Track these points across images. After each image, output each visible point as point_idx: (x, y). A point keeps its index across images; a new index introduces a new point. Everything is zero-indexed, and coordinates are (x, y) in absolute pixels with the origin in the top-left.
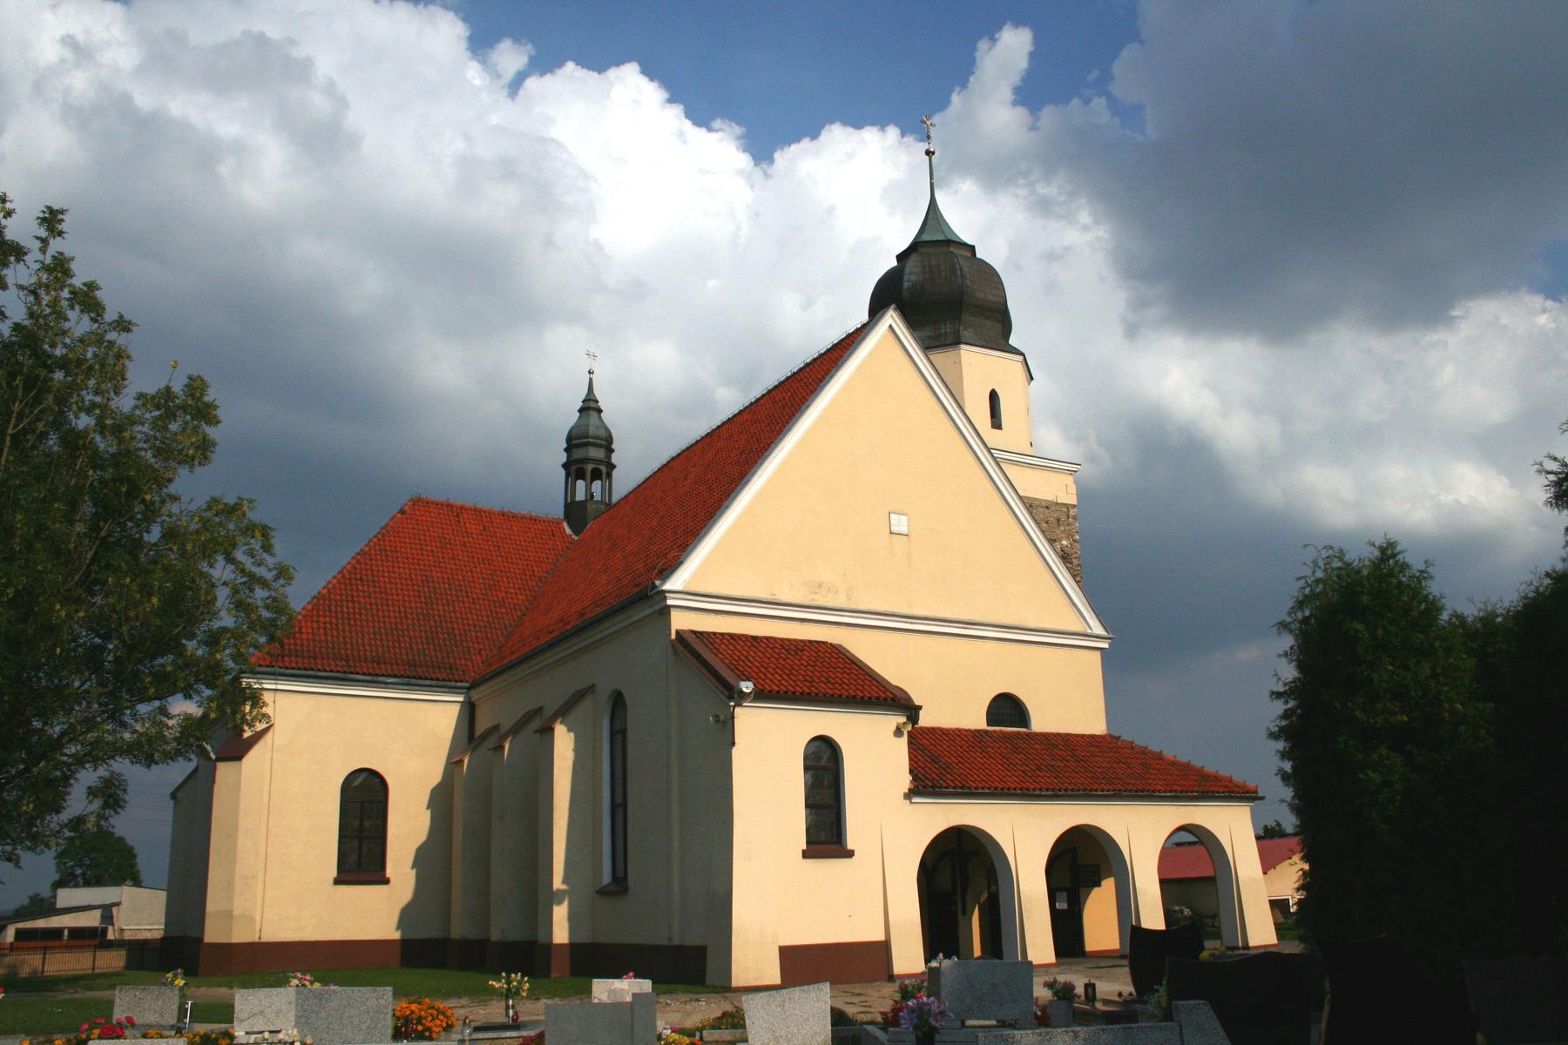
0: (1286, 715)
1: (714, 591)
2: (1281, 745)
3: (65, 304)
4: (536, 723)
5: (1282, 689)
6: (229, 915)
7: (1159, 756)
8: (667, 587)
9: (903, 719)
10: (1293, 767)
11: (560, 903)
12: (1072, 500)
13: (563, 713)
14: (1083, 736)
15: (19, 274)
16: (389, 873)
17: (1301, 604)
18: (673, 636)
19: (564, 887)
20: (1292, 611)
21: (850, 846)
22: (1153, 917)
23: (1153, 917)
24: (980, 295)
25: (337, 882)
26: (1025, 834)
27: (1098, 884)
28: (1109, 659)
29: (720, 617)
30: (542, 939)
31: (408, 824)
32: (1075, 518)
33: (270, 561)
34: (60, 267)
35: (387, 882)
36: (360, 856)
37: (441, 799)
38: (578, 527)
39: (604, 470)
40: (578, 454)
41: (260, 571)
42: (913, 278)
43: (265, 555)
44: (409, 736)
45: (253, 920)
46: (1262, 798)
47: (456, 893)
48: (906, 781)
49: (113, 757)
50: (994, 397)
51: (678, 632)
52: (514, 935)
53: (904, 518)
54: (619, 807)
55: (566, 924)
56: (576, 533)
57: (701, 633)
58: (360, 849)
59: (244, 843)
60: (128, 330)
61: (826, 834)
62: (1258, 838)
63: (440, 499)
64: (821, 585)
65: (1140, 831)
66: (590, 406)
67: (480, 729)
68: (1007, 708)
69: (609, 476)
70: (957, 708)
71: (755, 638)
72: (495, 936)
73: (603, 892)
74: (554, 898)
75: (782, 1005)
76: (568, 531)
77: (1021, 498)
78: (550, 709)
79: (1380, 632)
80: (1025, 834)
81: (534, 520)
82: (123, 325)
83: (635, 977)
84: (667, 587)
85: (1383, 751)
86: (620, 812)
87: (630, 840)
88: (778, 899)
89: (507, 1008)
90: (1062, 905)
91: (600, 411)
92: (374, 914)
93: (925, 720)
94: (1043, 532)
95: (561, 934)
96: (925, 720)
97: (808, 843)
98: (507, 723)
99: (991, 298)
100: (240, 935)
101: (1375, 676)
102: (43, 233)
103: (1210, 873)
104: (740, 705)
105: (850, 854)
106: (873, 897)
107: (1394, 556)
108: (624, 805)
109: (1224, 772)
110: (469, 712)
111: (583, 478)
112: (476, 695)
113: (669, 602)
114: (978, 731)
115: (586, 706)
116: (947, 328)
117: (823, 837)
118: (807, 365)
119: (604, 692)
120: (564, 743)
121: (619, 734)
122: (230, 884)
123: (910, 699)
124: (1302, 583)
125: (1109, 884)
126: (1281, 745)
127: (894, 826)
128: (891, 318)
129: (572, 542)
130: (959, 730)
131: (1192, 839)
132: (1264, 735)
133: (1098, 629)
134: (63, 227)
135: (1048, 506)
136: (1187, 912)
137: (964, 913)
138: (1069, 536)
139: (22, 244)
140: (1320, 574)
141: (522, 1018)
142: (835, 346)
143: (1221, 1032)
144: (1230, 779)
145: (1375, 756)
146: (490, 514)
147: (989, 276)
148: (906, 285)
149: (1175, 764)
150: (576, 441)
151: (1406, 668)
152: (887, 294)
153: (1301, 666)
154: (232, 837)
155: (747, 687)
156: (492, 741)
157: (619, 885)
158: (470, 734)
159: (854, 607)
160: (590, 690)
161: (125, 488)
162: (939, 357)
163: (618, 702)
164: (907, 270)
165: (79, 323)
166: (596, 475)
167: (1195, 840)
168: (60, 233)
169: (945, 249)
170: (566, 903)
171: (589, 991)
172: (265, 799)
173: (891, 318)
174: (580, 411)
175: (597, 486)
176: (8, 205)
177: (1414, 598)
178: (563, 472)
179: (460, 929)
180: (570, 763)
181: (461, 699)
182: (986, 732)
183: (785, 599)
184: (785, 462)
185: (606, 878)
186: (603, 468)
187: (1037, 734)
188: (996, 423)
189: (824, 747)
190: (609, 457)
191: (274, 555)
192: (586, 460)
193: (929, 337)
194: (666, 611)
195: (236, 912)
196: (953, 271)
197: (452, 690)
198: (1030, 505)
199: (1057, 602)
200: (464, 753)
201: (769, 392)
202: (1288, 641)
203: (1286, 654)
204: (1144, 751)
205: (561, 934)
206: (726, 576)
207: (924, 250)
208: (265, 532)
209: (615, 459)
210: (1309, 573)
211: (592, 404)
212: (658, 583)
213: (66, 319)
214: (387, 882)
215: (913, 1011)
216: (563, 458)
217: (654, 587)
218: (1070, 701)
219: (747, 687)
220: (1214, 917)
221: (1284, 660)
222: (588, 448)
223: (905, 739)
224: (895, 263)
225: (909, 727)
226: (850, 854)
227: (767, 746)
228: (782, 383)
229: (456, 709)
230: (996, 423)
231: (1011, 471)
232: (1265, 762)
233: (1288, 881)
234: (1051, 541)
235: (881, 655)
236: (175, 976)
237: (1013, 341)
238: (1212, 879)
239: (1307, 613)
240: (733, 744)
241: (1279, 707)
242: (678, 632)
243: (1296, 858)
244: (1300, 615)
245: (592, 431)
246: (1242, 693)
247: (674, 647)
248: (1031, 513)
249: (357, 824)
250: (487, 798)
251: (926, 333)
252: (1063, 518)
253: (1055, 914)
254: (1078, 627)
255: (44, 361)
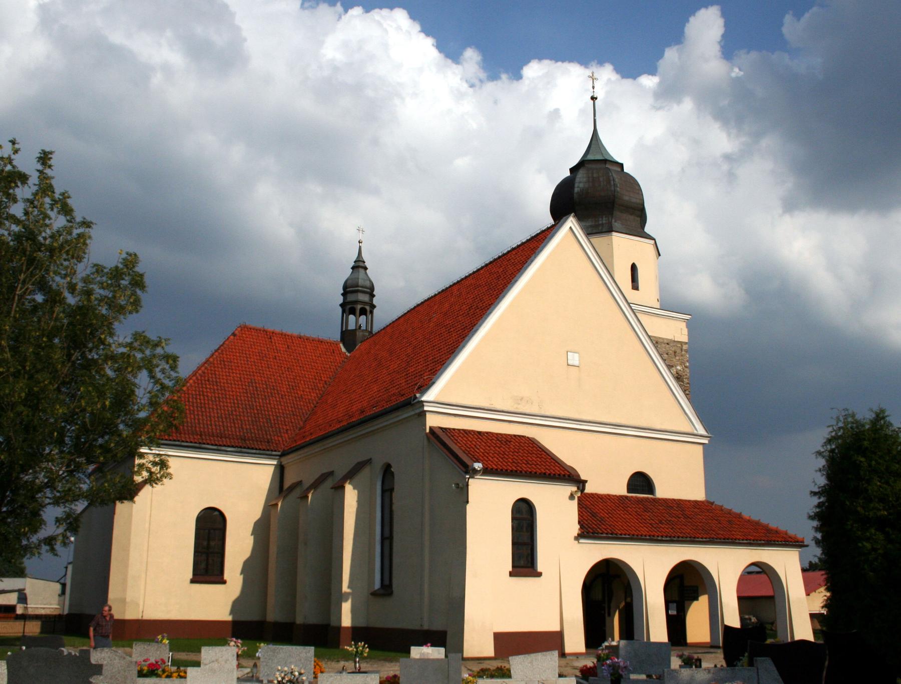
0: (819, 505)
1: (454, 402)
2: (815, 523)
3: (47, 206)
4: (329, 483)
5: (817, 490)
6: (123, 601)
7: (739, 516)
8: (424, 398)
9: (574, 489)
10: (822, 537)
11: (346, 600)
12: (684, 338)
13: (350, 476)
14: (689, 501)
15: (23, 192)
16: (226, 577)
17: (829, 441)
18: (428, 431)
19: (349, 590)
20: (825, 444)
21: (539, 569)
22: (732, 619)
23: (732, 619)
24: (626, 198)
25: (193, 581)
26: (651, 565)
27: (696, 599)
28: (708, 452)
29: (457, 419)
30: (333, 623)
31: (238, 546)
32: (686, 351)
33: (174, 374)
34: (45, 188)
35: (224, 582)
36: (207, 565)
37: (262, 529)
38: (350, 347)
39: (367, 309)
40: (351, 298)
41: (167, 382)
42: (581, 185)
43: (172, 373)
44: (240, 485)
45: (138, 605)
46: (807, 546)
47: (272, 590)
48: (575, 529)
49: (77, 500)
50: (634, 268)
51: (430, 428)
52: (313, 620)
53: (576, 355)
54: (387, 539)
55: (349, 615)
56: (349, 352)
57: (446, 429)
58: (207, 560)
59: (134, 555)
60: (90, 227)
61: (524, 561)
62: (804, 570)
63: (259, 325)
64: (522, 399)
65: (726, 565)
66: (359, 265)
67: (287, 485)
68: (641, 482)
69: (371, 312)
70: (610, 483)
71: (480, 433)
72: (299, 620)
73: (374, 594)
74: (342, 597)
75: (531, 662)
76: (344, 350)
77: (649, 337)
78: (340, 473)
79: (873, 463)
80: (651, 565)
81: (321, 342)
82: (87, 224)
83: (432, 646)
84: (424, 398)
85: (873, 531)
86: (387, 543)
87: (396, 560)
88: (492, 602)
89: (355, 662)
90: (673, 612)
91: (366, 268)
92: (215, 603)
93: (589, 489)
94: (664, 360)
95: (346, 621)
96: (589, 489)
97: (513, 567)
98: (308, 481)
99: (634, 200)
100: (130, 614)
101: (870, 488)
102: (40, 167)
103: (770, 593)
104: (473, 477)
105: (539, 575)
106: (554, 601)
107: (883, 418)
108: (391, 538)
109: (782, 528)
110: (281, 471)
111: (354, 314)
112: (285, 460)
113: (426, 408)
114: (621, 496)
115: (366, 473)
116: (604, 220)
117: (522, 563)
118: (513, 249)
119: (378, 466)
120: (351, 496)
121: (387, 491)
122: (124, 581)
123: (579, 476)
124: (830, 429)
125: (704, 600)
126: (815, 523)
127: (567, 557)
128: (571, 222)
129: (347, 357)
130: (609, 495)
131: (759, 570)
132: (806, 516)
133: (702, 431)
134: (52, 162)
135: (668, 343)
136: (754, 619)
137: (609, 615)
138: (682, 363)
139: (27, 173)
140: (841, 424)
141: (362, 670)
142: (533, 238)
143: (776, 672)
144: (786, 533)
145: (868, 534)
146: (291, 337)
147: (632, 184)
148: (576, 190)
149: (749, 521)
150: (349, 289)
151: (887, 483)
152: (565, 202)
153: (829, 477)
154: (126, 549)
155: (478, 466)
156: (297, 492)
157: (386, 590)
158: (281, 487)
159: (543, 413)
160: (369, 462)
161: (85, 327)
162: (598, 240)
163: (387, 472)
164: (577, 180)
165: (58, 222)
166: (363, 312)
167: (760, 572)
168: (50, 167)
169: (603, 166)
170: (350, 601)
171: (409, 652)
172: (147, 525)
173: (571, 222)
174: (353, 268)
175: (363, 319)
176: (17, 146)
177: (894, 443)
178: (340, 310)
179: (273, 615)
180: (355, 510)
181: (275, 462)
182: (626, 497)
183: (499, 407)
184: (501, 318)
185: (377, 585)
186: (368, 308)
187: (659, 499)
188: (635, 285)
189: (524, 506)
190: (372, 300)
191: (176, 372)
192: (356, 302)
193: (591, 226)
194: (423, 414)
195: (128, 600)
196: (609, 181)
197: (270, 457)
198: (656, 342)
199: (674, 411)
200: (277, 498)
201: (487, 265)
202: (822, 462)
203: (820, 470)
204: (730, 512)
205: (346, 621)
206: (465, 391)
207: (590, 166)
208: (175, 359)
209: (375, 301)
210: (835, 423)
211: (361, 264)
212: (418, 395)
213: (50, 219)
214: (224, 582)
215: (609, 666)
216: (341, 300)
217: (416, 398)
218: (681, 478)
219: (478, 466)
220: (772, 623)
221: (819, 474)
222: (357, 295)
223: (576, 501)
224: (568, 174)
225: (579, 494)
226: (539, 575)
227: (489, 503)
228: (495, 260)
229: (272, 469)
230: (635, 285)
231: (639, 315)
232: (808, 530)
233: (818, 601)
234: (670, 367)
235: (560, 445)
236: (163, 638)
237: (647, 229)
238: (772, 598)
239: (833, 447)
240: (468, 502)
241: (816, 500)
242: (430, 428)
243: (822, 589)
244: (829, 447)
245: (361, 282)
246: (793, 481)
247: (428, 439)
248: (656, 347)
249: (205, 543)
250: (295, 531)
251: (589, 223)
252: (678, 351)
253: (669, 618)
254: (688, 428)
255: (39, 247)
